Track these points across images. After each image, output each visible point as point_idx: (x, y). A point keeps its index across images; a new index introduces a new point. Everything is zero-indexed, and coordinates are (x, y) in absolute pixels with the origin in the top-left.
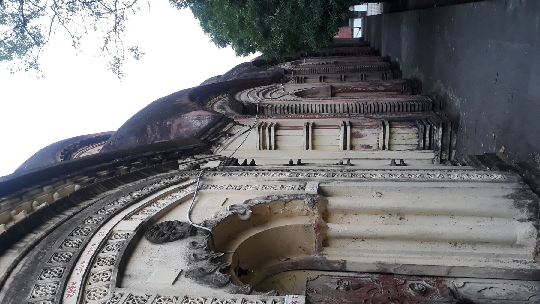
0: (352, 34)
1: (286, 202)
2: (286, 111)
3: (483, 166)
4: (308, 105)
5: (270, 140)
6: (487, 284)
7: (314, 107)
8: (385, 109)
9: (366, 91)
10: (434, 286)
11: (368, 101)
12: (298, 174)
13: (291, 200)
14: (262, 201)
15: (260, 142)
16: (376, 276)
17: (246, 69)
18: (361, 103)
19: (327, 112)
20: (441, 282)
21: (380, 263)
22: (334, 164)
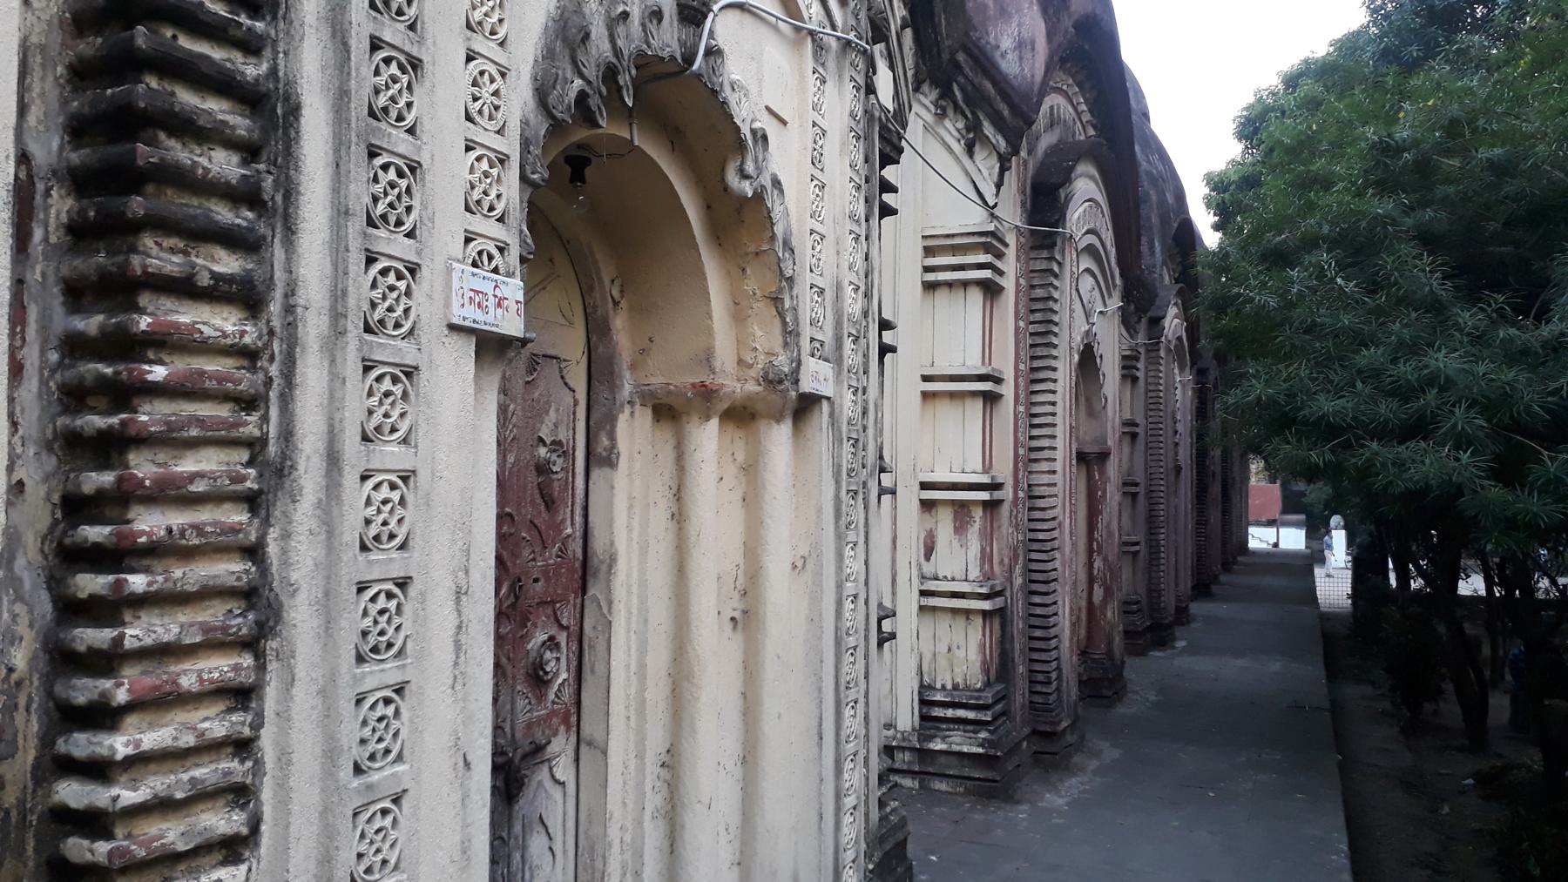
0: (1258, 524)
1: (776, 300)
2: (1038, 316)
3: (877, 856)
4: (1055, 381)
5: (951, 267)
6: (563, 841)
7: (1050, 397)
8: (1037, 599)
9: (1090, 552)
10: (553, 702)
11: (1063, 555)
12: (856, 340)
13: (781, 315)
14: (779, 230)
15: (948, 236)
16: (576, 547)
17: (1170, 199)
18: (1055, 534)
19: (1031, 438)
20: (565, 721)
21: (612, 560)
22: (881, 449)
